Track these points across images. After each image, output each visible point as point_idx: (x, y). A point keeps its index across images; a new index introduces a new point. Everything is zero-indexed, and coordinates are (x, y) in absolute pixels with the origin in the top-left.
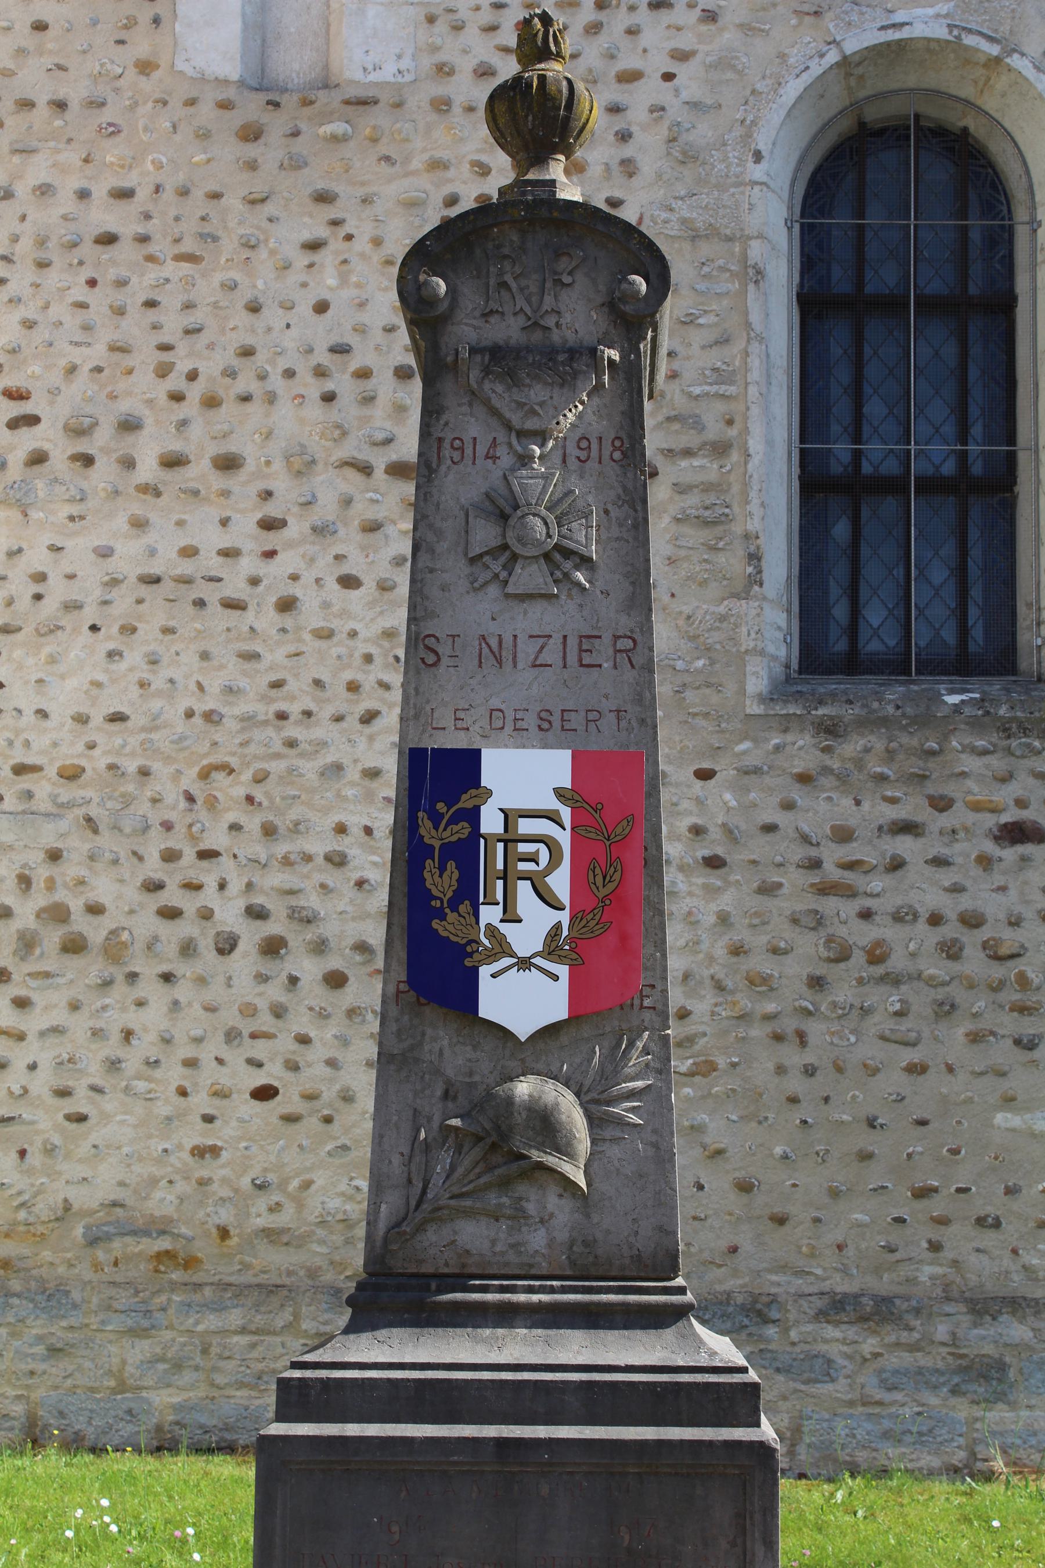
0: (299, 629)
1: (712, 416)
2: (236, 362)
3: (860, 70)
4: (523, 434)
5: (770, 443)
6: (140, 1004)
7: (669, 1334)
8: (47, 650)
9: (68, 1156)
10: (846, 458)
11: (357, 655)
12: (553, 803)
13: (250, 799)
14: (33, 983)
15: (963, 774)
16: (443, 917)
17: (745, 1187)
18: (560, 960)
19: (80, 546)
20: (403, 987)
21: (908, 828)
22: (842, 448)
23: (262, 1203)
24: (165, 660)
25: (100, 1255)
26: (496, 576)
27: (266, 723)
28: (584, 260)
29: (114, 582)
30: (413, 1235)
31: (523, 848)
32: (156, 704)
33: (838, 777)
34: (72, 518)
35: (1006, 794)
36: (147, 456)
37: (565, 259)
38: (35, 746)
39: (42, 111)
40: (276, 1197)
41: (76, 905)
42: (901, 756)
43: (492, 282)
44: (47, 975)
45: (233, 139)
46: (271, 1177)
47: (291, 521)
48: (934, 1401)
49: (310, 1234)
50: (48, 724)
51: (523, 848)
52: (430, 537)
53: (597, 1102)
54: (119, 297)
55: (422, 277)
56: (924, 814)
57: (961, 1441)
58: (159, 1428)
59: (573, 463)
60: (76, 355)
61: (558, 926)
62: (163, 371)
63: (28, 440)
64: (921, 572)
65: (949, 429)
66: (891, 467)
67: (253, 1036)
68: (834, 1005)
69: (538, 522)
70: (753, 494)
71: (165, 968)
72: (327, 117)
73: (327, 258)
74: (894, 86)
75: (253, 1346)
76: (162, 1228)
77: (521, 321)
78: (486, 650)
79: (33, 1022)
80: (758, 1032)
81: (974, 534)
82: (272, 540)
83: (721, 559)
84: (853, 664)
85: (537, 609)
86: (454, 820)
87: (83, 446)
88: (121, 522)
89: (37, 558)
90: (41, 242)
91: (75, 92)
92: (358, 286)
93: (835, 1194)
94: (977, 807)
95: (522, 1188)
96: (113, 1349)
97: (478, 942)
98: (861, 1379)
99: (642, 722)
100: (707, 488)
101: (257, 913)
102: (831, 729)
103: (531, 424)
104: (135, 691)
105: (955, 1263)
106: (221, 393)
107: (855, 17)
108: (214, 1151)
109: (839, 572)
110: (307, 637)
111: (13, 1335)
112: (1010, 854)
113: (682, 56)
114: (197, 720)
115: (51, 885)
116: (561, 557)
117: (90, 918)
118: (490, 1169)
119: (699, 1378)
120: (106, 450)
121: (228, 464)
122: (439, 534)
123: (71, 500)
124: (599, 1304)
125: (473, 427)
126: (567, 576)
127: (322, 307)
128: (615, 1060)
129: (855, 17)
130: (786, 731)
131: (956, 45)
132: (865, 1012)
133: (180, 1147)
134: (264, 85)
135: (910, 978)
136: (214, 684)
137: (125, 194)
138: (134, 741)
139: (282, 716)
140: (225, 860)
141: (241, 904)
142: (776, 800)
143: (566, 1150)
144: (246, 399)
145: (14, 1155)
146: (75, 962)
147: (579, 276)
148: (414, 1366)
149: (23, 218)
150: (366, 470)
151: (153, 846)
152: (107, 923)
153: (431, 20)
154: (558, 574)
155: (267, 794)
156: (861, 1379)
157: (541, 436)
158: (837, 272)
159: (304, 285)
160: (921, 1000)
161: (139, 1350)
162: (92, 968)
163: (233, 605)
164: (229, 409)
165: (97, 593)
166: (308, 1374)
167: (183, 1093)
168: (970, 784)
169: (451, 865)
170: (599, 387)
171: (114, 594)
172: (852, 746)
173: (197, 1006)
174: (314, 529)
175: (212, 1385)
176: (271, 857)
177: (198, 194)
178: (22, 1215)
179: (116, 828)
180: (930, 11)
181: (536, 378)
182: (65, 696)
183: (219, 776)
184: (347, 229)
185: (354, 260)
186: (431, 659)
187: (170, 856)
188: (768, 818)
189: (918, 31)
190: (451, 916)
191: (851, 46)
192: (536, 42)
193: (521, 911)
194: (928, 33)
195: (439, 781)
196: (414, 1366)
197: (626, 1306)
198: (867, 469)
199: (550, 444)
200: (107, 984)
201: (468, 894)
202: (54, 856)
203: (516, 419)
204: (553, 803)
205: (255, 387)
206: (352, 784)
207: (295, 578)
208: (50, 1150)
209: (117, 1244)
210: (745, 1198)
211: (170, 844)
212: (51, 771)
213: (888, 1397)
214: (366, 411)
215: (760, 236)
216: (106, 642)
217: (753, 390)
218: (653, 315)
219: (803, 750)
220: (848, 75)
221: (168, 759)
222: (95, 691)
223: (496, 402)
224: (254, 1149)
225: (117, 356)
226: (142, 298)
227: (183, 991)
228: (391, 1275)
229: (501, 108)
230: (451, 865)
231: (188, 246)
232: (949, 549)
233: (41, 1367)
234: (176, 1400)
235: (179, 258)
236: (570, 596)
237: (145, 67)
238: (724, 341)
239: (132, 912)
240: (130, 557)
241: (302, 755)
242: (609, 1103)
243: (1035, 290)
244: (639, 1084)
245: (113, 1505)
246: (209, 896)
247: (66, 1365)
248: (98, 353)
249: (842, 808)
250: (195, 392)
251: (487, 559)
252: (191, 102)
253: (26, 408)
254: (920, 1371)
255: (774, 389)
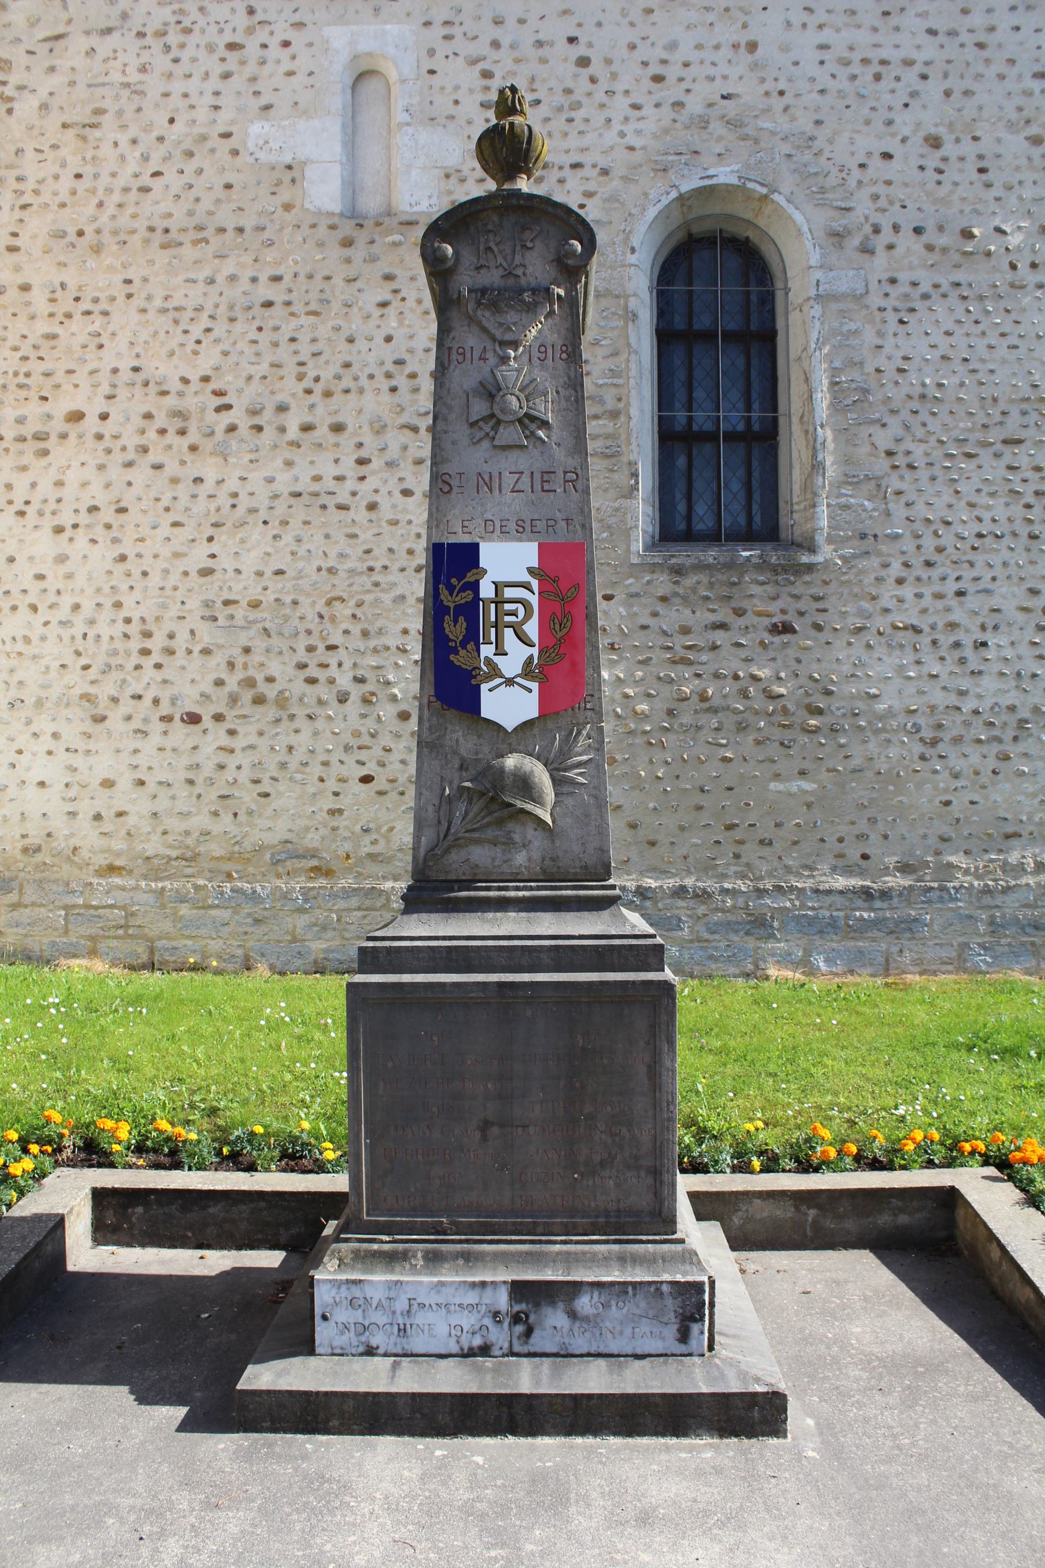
0: (379, 520)
1: (609, 396)
2: (341, 371)
3: (688, 203)
4: (504, 344)
5: (642, 411)
6: (297, 731)
7: (605, 914)
8: (240, 536)
9: (260, 816)
10: (684, 421)
11: (413, 534)
12: (527, 578)
13: (354, 616)
14: (237, 721)
15: (752, 596)
16: (457, 653)
17: (633, 826)
18: (533, 679)
19: (256, 477)
20: (433, 699)
21: (722, 626)
22: (681, 415)
23: (367, 839)
24: (305, 539)
25: (280, 869)
26: (487, 434)
27: (362, 573)
28: (540, 232)
29: (276, 496)
30: (442, 856)
31: (508, 607)
32: (301, 564)
33: (683, 598)
34: (251, 461)
35: (774, 607)
36: (293, 422)
37: (528, 232)
38: (234, 589)
39: (230, 233)
40: (375, 836)
41: (260, 678)
42: (717, 586)
43: (482, 247)
44: (245, 716)
45: (337, 246)
46: (371, 825)
47: (373, 459)
48: (736, 939)
49: (393, 856)
50: (242, 577)
51: (508, 607)
52: (445, 410)
53: (558, 770)
54: (275, 336)
55: (436, 245)
56: (729, 617)
57: (750, 960)
58: (315, 962)
59: (536, 361)
60: (252, 370)
61: (531, 657)
62: (300, 377)
63: (226, 418)
64: (726, 485)
65: (741, 405)
66: (709, 427)
67: (359, 748)
68: (682, 725)
69: (514, 399)
70: (633, 440)
71: (309, 711)
72: (389, 232)
73: (391, 311)
74: (709, 212)
75: (365, 917)
76: (313, 854)
77: (501, 272)
78: (481, 482)
79: (238, 743)
80: (639, 740)
81: (755, 463)
82: (363, 470)
83: (616, 476)
84: (689, 536)
85: (513, 455)
86: (463, 589)
87: (257, 421)
88: (279, 463)
89: (233, 484)
90: (231, 308)
91: (248, 222)
92: (409, 326)
93: (682, 828)
94: (759, 614)
95: (511, 826)
96: (289, 919)
97: (480, 669)
98: (696, 928)
99: (583, 526)
100: (608, 436)
101: (360, 680)
102: (678, 571)
103: (508, 337)
104: (289, 557)
105: (748, 865)
106: (333, 388)
107: (686, 172)
108: (340, 811)
109: (681, 485)
110: (384, 524)
111: (234, 912)
112: (777, 639)
113: (589, 195)
114: (324, 573)
115: (245, 666)
116: (530, 421)
117: (268, 684)
118: (490, 813)
119: (625, 942)
120: (269, 423)
121: (338, 428)
122: (450, 409)
123: (251, 451)
124: (561, 897)
125: (470, 339)
126: (533, 433)
127: (389, 339)
128: (569, 740)
129: (686, 172)
130: (653, 572)
131: (743, 188)
132: (699, 728)
133: (321, 810)
134: (355, 216)
135: (723, 709)
136: (333, 553)
137: (277, 279)
138: (289, 585)
139: (371, 569)
140: (341, 651)
141: (351, 674)
142: (648, 611)
143: (539, 801)
144: (347, 391)
145: (231, 816)
146: (260, 709)
147: (538, 242)
148: (444, 938)
149: (221, 294)
150: (415, 429)
151: (301, 644)
152: (277, 687)
153: (447, 176)
154: (527, 432)
155: (364, 613)
156: (696, 928)
157: (515, 344)
158: (677, 318)
159: (379, 327)
160: (729, 721)
161: (303, 920)
162: (270, 712)
163: (341, 507)
164: (338, 398)
165: (267, 503)
166: (378, 944)
167: (322, 780)
168: (755, 601)
169: (461, 619)
170: (551, 313)
171: (276, 503)
172: (690, 581)
173: (328, 732)
174: (387, 464)
175: (343, 938)
176: (366, 648)
177: (318, 277)
178: (237, 848)
179: (280, 634)
180: (728, 169)
181: (511, 307)
182: (250, 562)
183: (337, 603)
184: (403, 294)
185: (406, 312)
186: (446, 488)
187: (311, 649)
188: (644, 622)
189: (721, 180)
190: (462, 652)
191: (685, 188)
192: (508, 104)
193: (506, 648)
194: (727, 181)
195: (453, 565)
196: (444, 938)
197: (578, 898)
198: (695, 428)
199: (521, 349)
200: (278, 721)
201: (472, 637)
202: (247, 650)
203: (498, 333)
204: (527, 578)
205: (352, 385)
206: (412, 606)
207: (376, 491)
208: (250, 813)
209: (288, 863)
210: (633, 832)
211: (311, 642)
212: (244, 603)
213: (711, 937)
214: (415, 397)
215: (635, 295)
216: (274, 529)
217: (632, 381)
218: (586, 266)
219: (663, 583)
220: (683, 205)
221: (308, 595)
222: (267, 558)
223: (485, 323)
224: (362, 810)
225: (275, 369)
226: (288, 336)
227: (320, 724)
228: (428, 881)
229: (486, 144)
230: (461, 619)
231: (313, 307)
232: (741, 472)
233: (250, 929)
234: (324, 946)
235: (309, 313)
236: (535, 446)
237: (288, 207)
238: (615, 354)
239: (290, 680)
240: (284, 482)
241: (382, 591)
242: (566, 770)
243: (787, 326)
244: (585, 758)
245: (288, 1005)
246: (333, 671)
247: (264, 929)
248: (264, 368)
249: (685, 616)
250: (318, 389)
251: (481, 423)
252: (314, 226)
253: (225, 400)
254: (729, 923)
255: (644, 381)
